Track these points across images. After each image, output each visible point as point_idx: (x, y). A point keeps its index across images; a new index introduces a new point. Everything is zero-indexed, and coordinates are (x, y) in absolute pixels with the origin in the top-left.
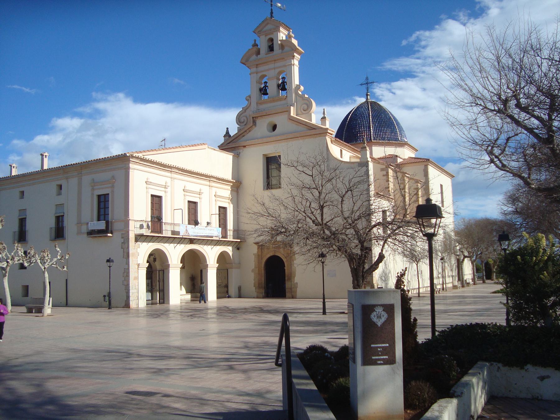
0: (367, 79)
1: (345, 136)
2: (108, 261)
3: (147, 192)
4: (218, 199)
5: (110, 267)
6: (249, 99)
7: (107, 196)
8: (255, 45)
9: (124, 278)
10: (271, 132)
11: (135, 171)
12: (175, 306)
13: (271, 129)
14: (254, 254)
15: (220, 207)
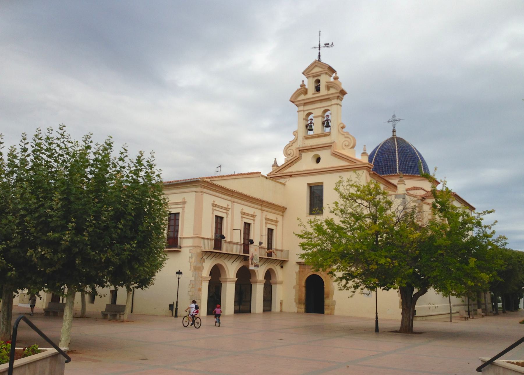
0: (394, 116)
2: (177, 273)
3: (213, 213)
4: (268, 222)
5: (179, 278)
6: (296, 133)
7: (177, 214)
8: (303, 86)
11: (204, 194)
13: (315, 161)
14: (296, 272)
15: (269, 229)
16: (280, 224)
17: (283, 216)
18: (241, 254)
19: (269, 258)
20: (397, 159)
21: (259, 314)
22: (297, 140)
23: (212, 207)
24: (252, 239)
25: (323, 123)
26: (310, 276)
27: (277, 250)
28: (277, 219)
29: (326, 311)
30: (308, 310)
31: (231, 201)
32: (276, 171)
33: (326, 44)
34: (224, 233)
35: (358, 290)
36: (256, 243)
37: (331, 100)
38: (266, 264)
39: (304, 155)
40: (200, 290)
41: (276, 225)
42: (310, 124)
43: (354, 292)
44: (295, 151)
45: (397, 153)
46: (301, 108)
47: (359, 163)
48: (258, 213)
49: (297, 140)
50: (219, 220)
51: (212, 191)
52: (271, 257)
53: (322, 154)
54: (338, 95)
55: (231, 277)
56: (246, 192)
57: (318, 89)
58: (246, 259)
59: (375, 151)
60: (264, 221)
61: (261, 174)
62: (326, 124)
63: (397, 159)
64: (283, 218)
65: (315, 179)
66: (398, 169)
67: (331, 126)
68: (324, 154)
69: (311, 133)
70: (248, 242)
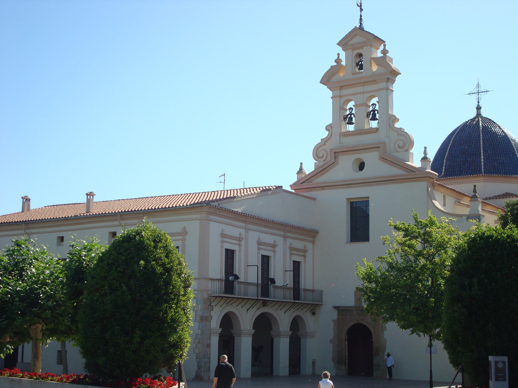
0: (478, 86)
1: (446, 166)
3: (222, 246)
8: (338, 61)
9: (195, 344)
10: (358, 172)
11: (211, 222)
13: (357, 167)
14: (333, 321)
16: (309, 255)
17: (313, 243)
18: (259, 298)
19: (296, 301)
21: (284, 377)
23: (220, 238)
24: (272, 277)
27: (305, 290)
31: (244, 228)
34: (236, 272)
37: (378, 83)
38: (292, 310)
40: (209, 346)
41: (305, 256)
42: (349, 116)
48: (280, 241)
50: (230, 255)
51: (221, 217)
52: (299, 300)
53: (365, 157)
59: (450, 140)
60: (288, 251)
61: (283, 188)
64: (313, 246)
65: (358, 193)
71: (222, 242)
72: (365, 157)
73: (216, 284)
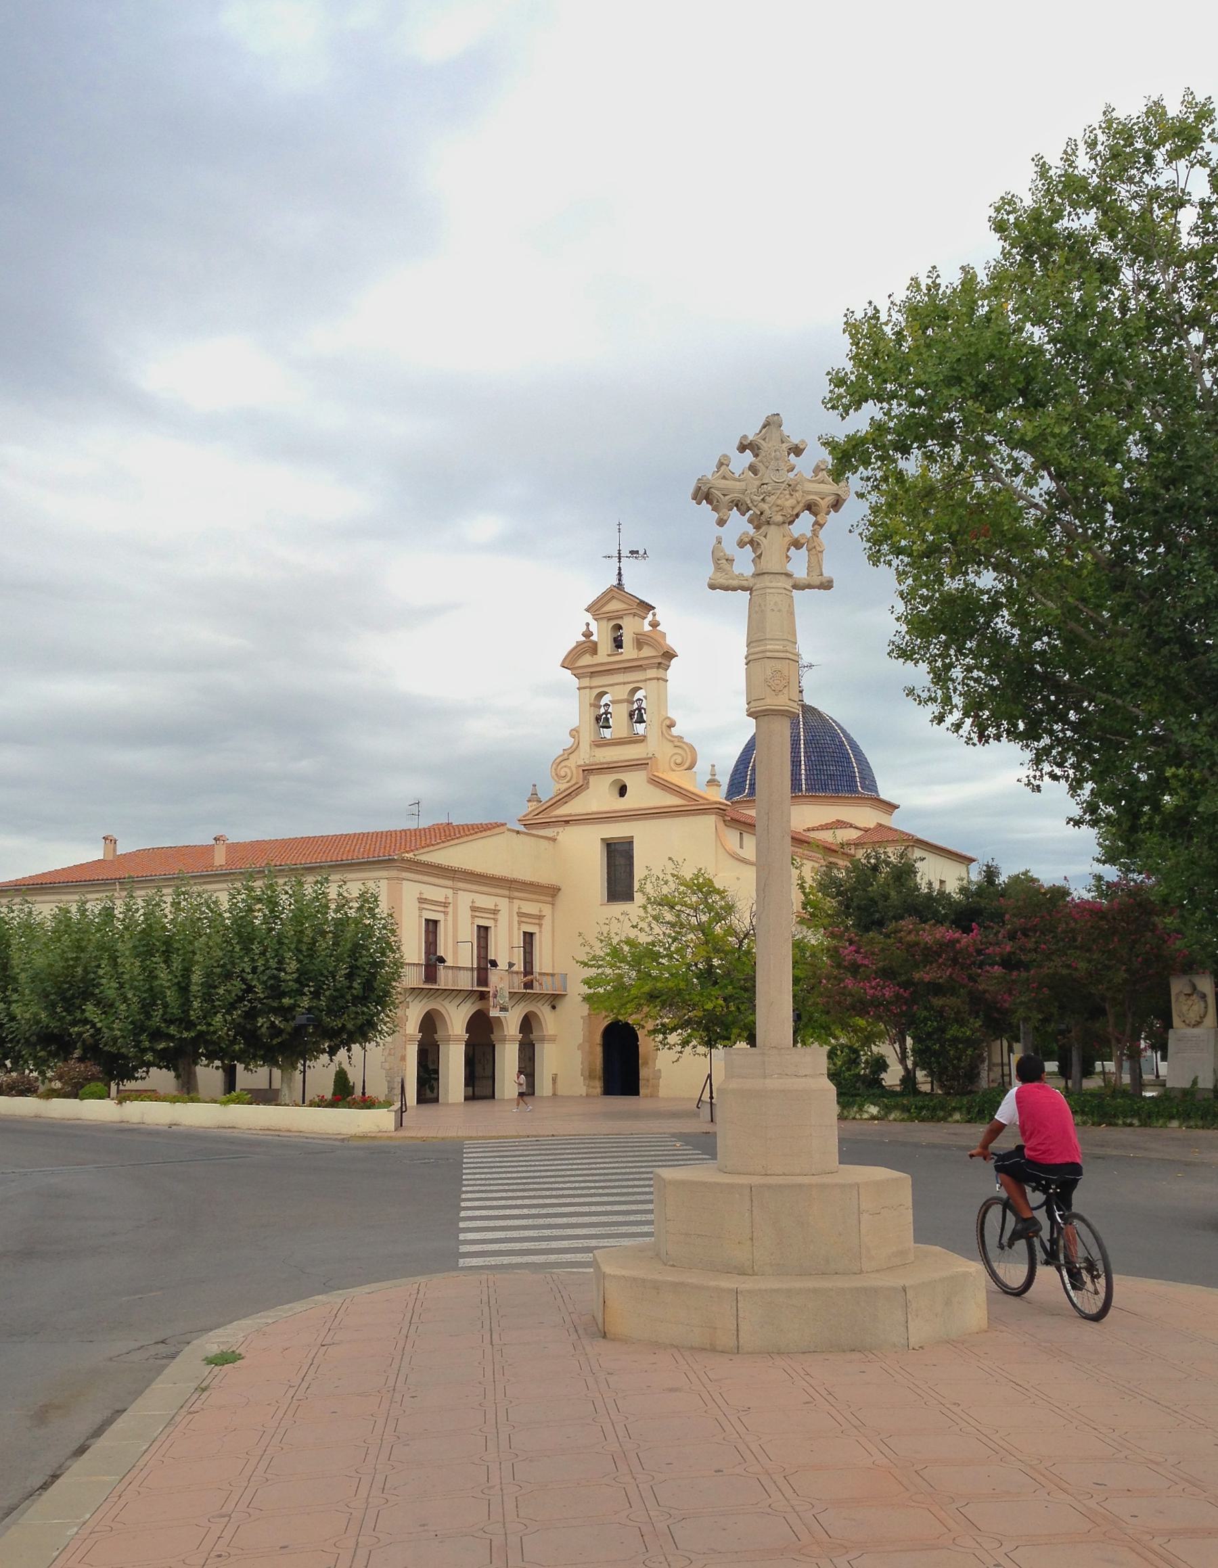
3: (420, 916)
8: (588, 634)
12: (363, 1137)
14: (582, 1017)
16: (546, 923)
17: (553, 904)
20: (803, 758)
22: (577, 747)
23: (417, 904)
25: (631, 715)
26: (610, 1025)
27: (540, 974)
28: (540, 911)
29: (641, 1091)
30: (608, 1090)
32: (536, 812)
33: (632, 552)
35: (688, 1049)
36: (503, 964)
37: (645, 669)
38: (523, 1004)
39: (593, 779)
40: (403, 1058)
41: (540, 925)
43: (681, 1052)
44: (574, 770)
45: (802, 746)
46: (586, 682)
47: (702, 801)
48: (503, 903)
49: (577, 747)
50: (432, 926)
52: (532, 989)
53: (628, 778)
54: (660, 660)
55: (456, 1033)
56: (479, 869)
57: (618, 643)
58: (483, 996)
60: (516, 918)
62: (637, 716)
63: (803, 758)
65: (617, 831)
66: (803, 782)
67: (648, 722)
68: (634, 780)
69: (607, 733)
70: (485, 965)
71: (421, 909)
72: (628, 778)
73: (469, 1177)
